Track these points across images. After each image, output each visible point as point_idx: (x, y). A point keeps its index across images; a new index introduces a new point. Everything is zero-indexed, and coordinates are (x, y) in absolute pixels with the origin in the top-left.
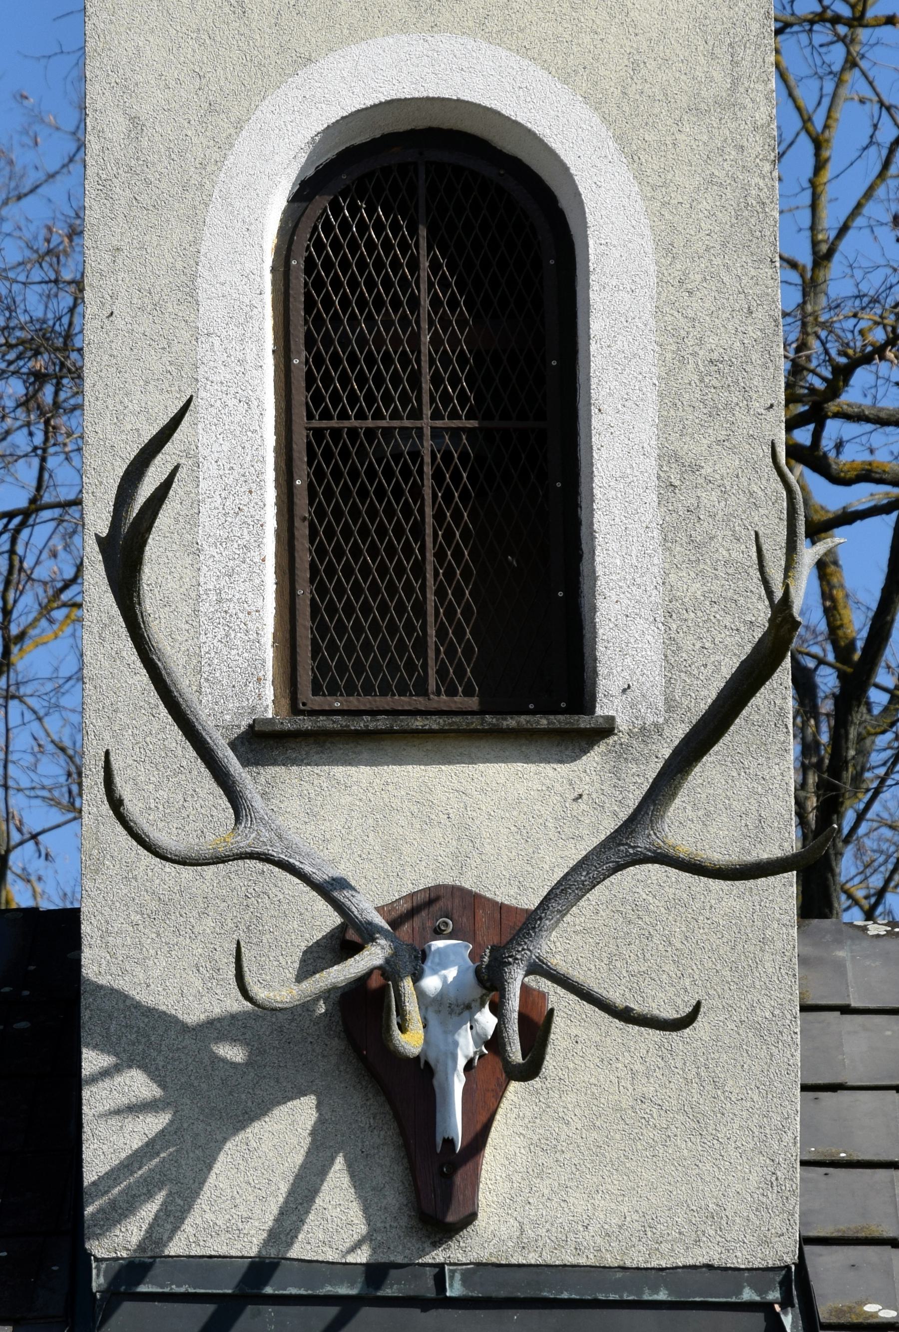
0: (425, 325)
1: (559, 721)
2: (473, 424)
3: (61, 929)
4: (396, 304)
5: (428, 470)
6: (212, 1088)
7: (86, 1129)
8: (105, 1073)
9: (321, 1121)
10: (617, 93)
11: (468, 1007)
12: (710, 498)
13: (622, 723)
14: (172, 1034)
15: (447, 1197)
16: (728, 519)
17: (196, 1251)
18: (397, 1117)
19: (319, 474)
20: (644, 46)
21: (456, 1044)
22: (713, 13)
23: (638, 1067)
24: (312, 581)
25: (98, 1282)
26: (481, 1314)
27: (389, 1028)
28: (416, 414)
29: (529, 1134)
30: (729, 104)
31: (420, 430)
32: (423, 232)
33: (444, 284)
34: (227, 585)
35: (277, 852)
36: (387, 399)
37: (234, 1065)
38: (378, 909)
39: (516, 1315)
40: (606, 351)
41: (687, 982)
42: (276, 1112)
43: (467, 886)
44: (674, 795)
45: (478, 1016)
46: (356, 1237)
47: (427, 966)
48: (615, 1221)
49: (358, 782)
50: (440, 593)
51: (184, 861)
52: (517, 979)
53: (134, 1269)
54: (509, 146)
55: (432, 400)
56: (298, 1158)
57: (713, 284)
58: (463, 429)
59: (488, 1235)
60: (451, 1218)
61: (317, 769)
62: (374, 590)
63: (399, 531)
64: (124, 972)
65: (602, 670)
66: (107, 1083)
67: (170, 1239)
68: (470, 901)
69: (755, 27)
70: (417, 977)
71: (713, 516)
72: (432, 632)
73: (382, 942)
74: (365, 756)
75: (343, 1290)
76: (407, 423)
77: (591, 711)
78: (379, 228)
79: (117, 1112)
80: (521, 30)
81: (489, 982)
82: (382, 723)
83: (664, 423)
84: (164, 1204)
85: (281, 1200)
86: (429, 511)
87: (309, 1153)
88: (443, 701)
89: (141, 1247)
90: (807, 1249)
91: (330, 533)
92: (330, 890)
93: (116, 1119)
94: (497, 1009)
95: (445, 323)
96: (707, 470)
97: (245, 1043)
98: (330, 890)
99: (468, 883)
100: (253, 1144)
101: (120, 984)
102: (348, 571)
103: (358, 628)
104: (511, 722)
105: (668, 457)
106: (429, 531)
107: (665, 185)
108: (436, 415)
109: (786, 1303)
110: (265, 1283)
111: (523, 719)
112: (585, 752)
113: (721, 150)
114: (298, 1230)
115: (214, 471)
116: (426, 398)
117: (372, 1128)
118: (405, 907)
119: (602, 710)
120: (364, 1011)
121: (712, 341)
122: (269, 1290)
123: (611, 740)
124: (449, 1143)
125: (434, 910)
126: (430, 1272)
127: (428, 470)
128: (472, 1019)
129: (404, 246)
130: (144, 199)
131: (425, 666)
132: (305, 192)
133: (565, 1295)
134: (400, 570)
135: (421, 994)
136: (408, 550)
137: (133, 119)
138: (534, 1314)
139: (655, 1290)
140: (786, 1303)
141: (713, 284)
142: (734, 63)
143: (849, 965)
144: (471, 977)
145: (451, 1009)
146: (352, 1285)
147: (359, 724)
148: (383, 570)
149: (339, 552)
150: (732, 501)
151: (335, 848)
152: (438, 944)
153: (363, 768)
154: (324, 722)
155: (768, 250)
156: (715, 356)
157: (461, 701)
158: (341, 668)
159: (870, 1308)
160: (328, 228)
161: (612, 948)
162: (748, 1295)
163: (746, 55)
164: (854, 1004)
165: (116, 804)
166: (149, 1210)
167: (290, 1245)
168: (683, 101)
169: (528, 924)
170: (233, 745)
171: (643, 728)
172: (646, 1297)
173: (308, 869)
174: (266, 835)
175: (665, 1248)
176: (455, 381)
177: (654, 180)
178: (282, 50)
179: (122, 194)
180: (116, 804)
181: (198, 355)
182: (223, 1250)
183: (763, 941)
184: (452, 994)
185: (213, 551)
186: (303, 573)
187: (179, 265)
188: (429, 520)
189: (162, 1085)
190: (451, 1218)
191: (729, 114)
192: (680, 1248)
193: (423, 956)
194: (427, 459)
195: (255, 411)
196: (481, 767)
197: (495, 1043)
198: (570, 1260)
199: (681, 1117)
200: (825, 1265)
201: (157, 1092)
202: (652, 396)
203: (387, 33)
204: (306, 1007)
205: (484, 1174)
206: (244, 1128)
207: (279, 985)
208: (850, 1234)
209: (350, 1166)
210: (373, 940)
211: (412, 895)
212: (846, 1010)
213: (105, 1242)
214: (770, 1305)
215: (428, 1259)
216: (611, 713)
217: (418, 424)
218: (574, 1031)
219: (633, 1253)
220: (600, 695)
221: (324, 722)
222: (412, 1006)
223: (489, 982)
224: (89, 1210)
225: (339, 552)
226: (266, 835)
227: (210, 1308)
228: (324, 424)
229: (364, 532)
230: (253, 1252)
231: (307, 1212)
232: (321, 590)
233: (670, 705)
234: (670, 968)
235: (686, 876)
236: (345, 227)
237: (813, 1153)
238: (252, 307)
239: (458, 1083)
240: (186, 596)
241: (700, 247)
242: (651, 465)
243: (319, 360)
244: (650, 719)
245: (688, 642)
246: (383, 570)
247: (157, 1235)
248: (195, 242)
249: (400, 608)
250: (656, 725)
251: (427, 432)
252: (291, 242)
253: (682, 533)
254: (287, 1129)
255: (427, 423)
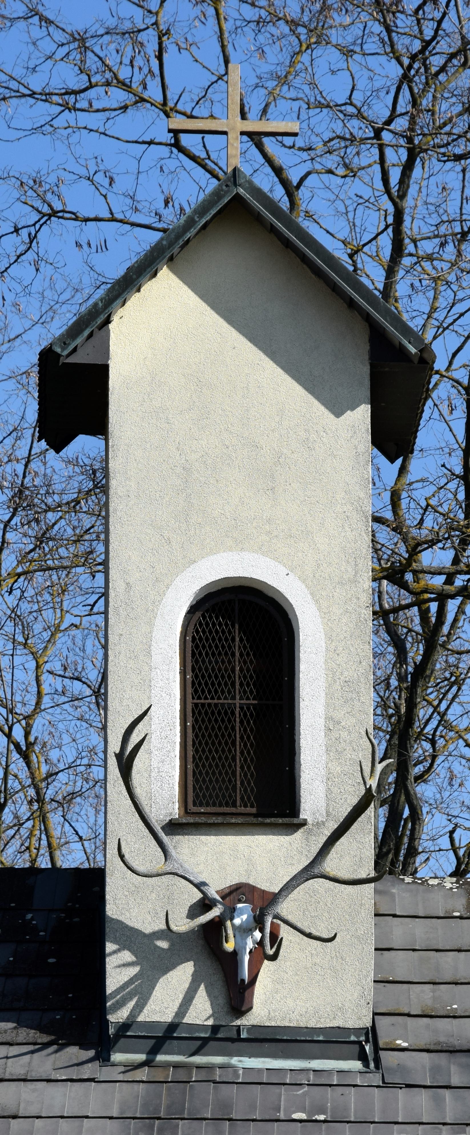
0: (237, 663)
1: (286, 820)
2: (256, 702)
3: (91, 882)
4: (226, 654)
5: (238, 720)
6: (155, 961)
7: (107, 973)
8: (115, 952)
9: (195, 971)
10: (312, 576)
11: (251, 930)
12: (344, 734)
13: (310, 821)
14: (140, 938)
15: (242, 1000)
16: (351, 742)
17: (148, 1020)
18: (223, 970)
19: (196, 721)
20: (322, 558)
21: (246, 944)
22: (348, 545)
23: (313, 952)
24: (193, 762)
25: (111, 1031)
26: (254, 1044)
27: (222, 943)
28: (233, 698)
29: (272, 977)
30: (354, 581)
31: (235, 704)
32: (237, 626)
33: (245, 647)
34: (162, 772)
35: (180, 872)
36: (223, 692)
37: (163, 949)
38: (217, 892)
39: (267, 1045)
40: (306, 677)
41: (332, 920)
42: (178, 968)
43: (251, 883)
44: (329, 853)
45: (254, 933)
46: (208, 1015)
47: (235, 914)
48: (304, 1010)
49: (210, 842)
50: (242, 768)
51: (146, 876)
52: (269, 920)
53: (125, 1026)
54: (270, 594)
55: (240, 692)
56: (187, 985)
57: (347, 651)
58: (252, 704)
59: (256, 1015)
60: (243, 1009)
61: (195, 837)
62: (217, 766)
63: (226, 743)
64: (122, 914)
65: (302, 800)
66: (115, 956)
67: (139, 1015)
68: (252, 889)
69: (364, 551)
70: (232, 919)
71: (345, 741)
72: (238, 783)
73: (220, 906)
74: (213, 832)
75: (203, 1035)
76: (230, 701)
77: (298, 816)
78: (220, 625)
79: (119, 966)
80: (275, 551)
81: (259, 922)
82: (220, 820)
83: (327, 705)
84: (137, 1002)
85: (180, 1001)
86: (238, 736)
87: (191, 983)
88: (242, 810)
89: (128, 1018)
90: (376, 1017)
91: (200, 743)
92: (200, 886)
93: (119, 969)
94: (262, 930)
95: (245, 662)
96: (343, 724)
97: (168, 941)
98: (200, 886)
99: (251, 882)
100: (170, 980)
101: (120, 918)
102: (207, 758)
103: (211, 781)
104: (268, 821)
105: (329, 718)
106: (238, 743)
107: (329, 612)
108: (241, 698)
109: (367, 1041)
110: (174, 1032)
111: (273, 819)
112: (296, 832)
113: (351, 599)
114: (186, 1012)
115: (157, 722)
116: (237, 692)
117: (214, 974)
118: (227, 891)
119: (302, 816)
120: (213, 932)
121: (346, 674)
122: (175, 1035)
123: (305, 827)
124: (243, 981)
125: (238, 892)
126: (235, 1029)
127: (238, 720)
128: (252, 935)
129: (230, 632)
130: (131, 615)
131: (236, 796)
132: (192, 610)
133: (285, 1038)
134: (227, 758)
135: (233, 925)
136: (230, 751)
137: (127, 584)
138: (274, 1044)
139: (319, 1036)
140: (367, 1041)
141: (347, 651)
142: (356, 565)
143: (397, 896)
144: (252, 919)
145: (245, 931)
146: (206, 1033)
147: (211, 821)
148: (220, 758)
149: (204, 751)
150: (353, 735)
151: (201, 867)
152: (240, 905)
153: (212, 837)
154: (198, 820)
155: (368, 638)
156: (347, 679)
157: (249, 810)
158: (204, 796)
159: (398, 1042)
160: (201, 624)
161: (305, 907)
162: (353, 1038)
163: (361, 562)
164: (398, 913)
165: (122, 856)
166: (131, 1004)
167: (183, 1018)
168: (336, 579)
169: (274, 899)
170: (163, 828)
171: (318, 823)
172: (315, 1039)
173: (192, 878)
174: (176, 866)
175: (322, 1020)
176: (248, 685)
177: (325, 610)
178: (185, 557)
179: (123, 613)
180: (122, 856)
181: (152, 681)
182: (158, 1020)
183: (361, 905)
184: (245, 925)
185: (157, 753)
186: (190, 759)
187: (144, 641)
188: (238, 739)
189: (136, 957)
190: (243, 1009)
191: (353, 585)
192: (328, 1020)
193: (234, 909)
194: (238, 715)
195: (173, 698)
196: (257, 837)
197: (261, 943)
198: (287, 1024)
199: (329, 971)
200: (383, 1023)
201: (134, 959)
202: (323, 694)
203: (224, 551)
204: (192, 931)
205: (255, 992)
206: (166, 973)
207: (182, 924)
208: (392, 1012)
209: (206, 988)
210: (216, 905)
211: (230, 886)
212: (395, 916)
213: (115, 1016)
214: (361, 1042)
215: (234, 1024)
216: (306, 817)
217: (234, 702)
218: (290, 938)
219: (310, 1022)
220: (302, 810)
221: (198, 820)
222: (230, 932)
223: (259, 922)
224: (108, 1004)
225: (204, 751)
226: (176, 866)
227: (153, 1041)
228: (199, 701)
229: (213, 744)
230: (170, 1020)
231: (190, 1006)
232: (197, 766)
233: (328, 814)
234: (326, 914)
235: (332, 883)
236: (207, 624)
237: (379, 977)
238: (172, 658)
239: (247, 958)
240: (146, 770)
241: (342, 637)
242: (322, 721)
243: (196, 676)
244: (320, 819)
245: (335, 790)
246: (220, 758)
247: (133, 1014)
248: (151, 632)
249: (227, 773)
250: (322, 821)
251: (238, 705)
252: (186, 630)
253: (334, 749)
254: (183, 973)
255: (237, 702)
